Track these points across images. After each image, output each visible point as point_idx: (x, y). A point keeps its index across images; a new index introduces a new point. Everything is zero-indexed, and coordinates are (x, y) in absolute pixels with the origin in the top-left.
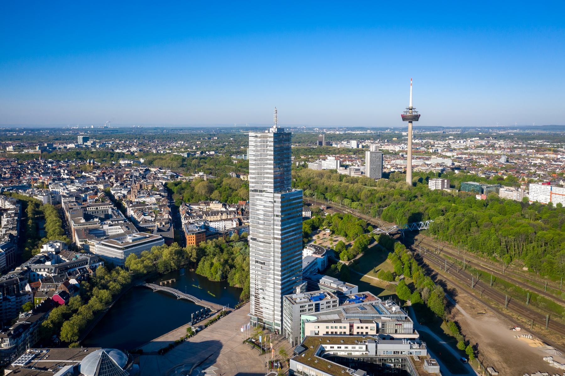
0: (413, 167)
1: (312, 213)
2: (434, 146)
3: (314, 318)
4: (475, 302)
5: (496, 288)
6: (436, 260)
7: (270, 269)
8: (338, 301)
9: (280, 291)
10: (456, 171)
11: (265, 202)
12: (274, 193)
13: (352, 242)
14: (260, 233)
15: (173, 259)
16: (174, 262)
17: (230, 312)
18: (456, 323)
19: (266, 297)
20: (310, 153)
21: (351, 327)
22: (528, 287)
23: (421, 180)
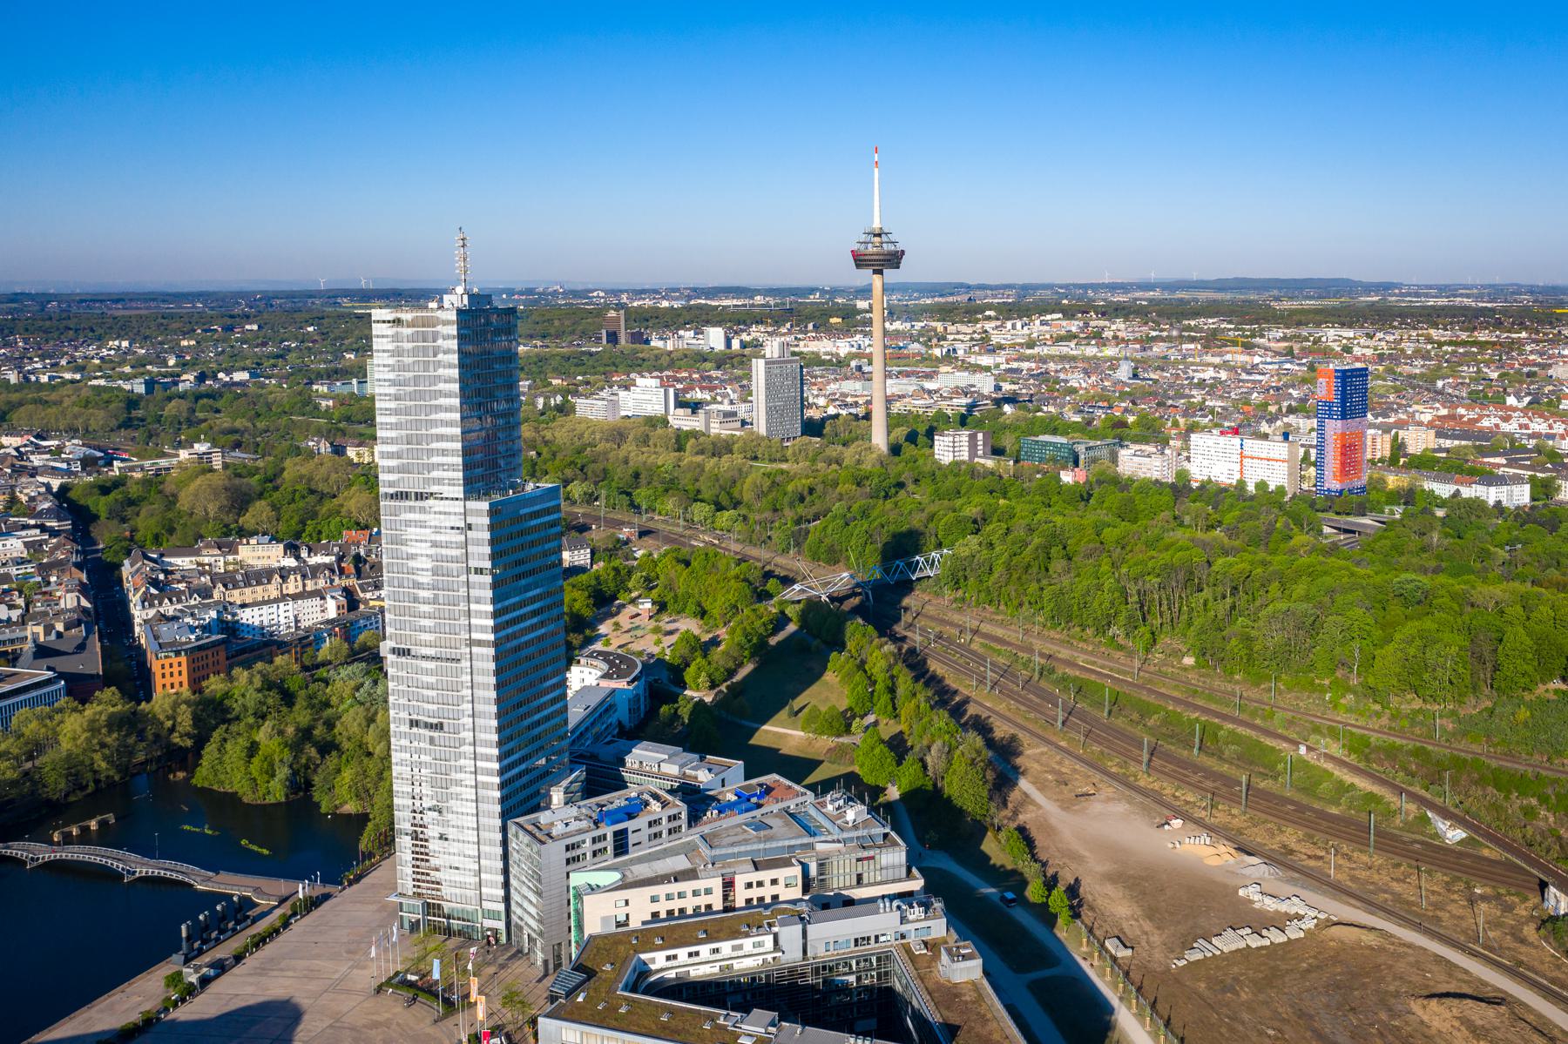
0: (889, 401)
1: (593, 553)
2: (945, 339)
3: (615, 877)
5: (1120, 722)
6: (961, 661)
7: (462, 742)
8: (684, 816)
9: (498, 808)
10: (1007, 408)
11: (437, 529)
12: (466, 499)
13: (722, 632)
14: (422, 629)
15: (103, 745)
16: (105, 758)
17: (326, 897)
18: (1022, 830)
19: (451, 833)
20: (581, 369)
21: (728, 885)
22: (1196, 708)
23: (912, 438)
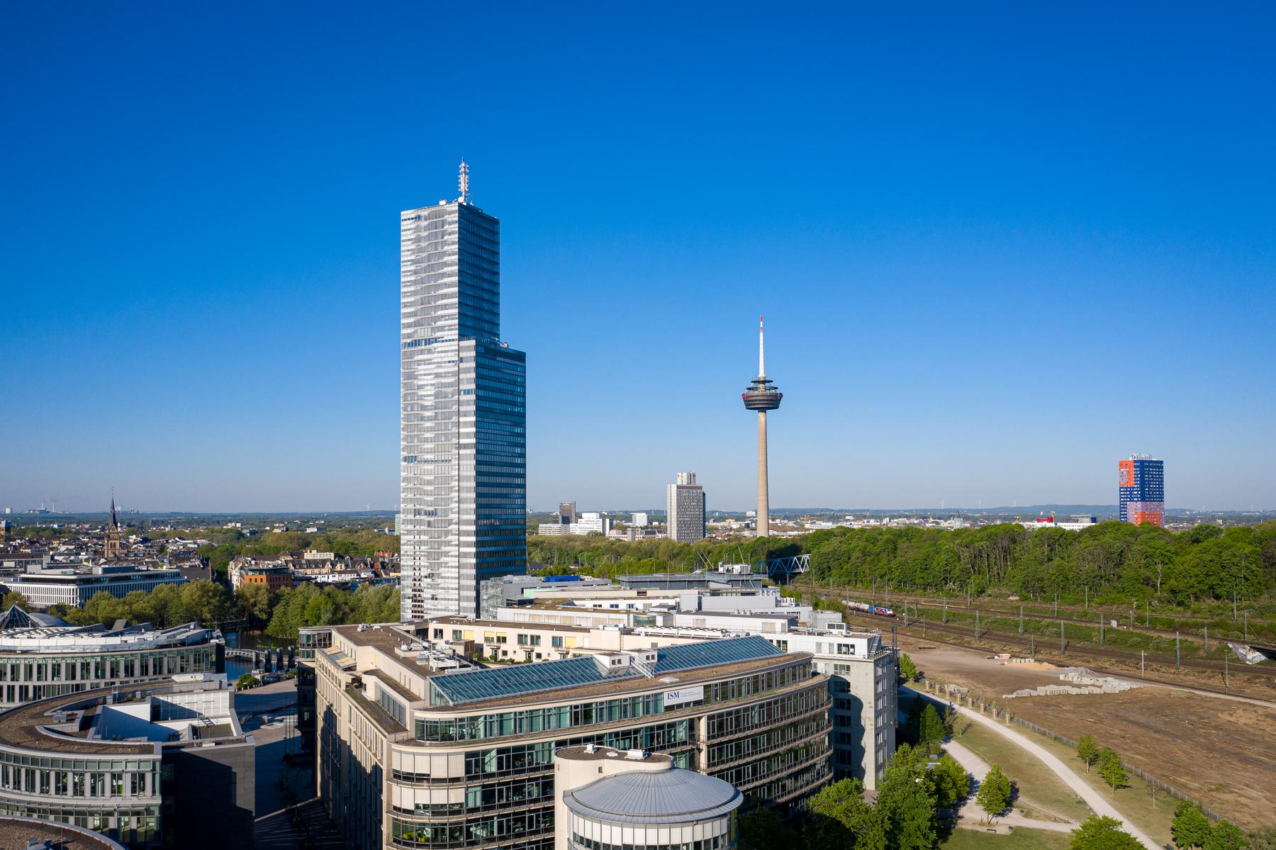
4: (912, 640)
5: (955, 625)
7: (450, 522)
9: (473, 572)
14: (426, 440)
15: (209, 603)
